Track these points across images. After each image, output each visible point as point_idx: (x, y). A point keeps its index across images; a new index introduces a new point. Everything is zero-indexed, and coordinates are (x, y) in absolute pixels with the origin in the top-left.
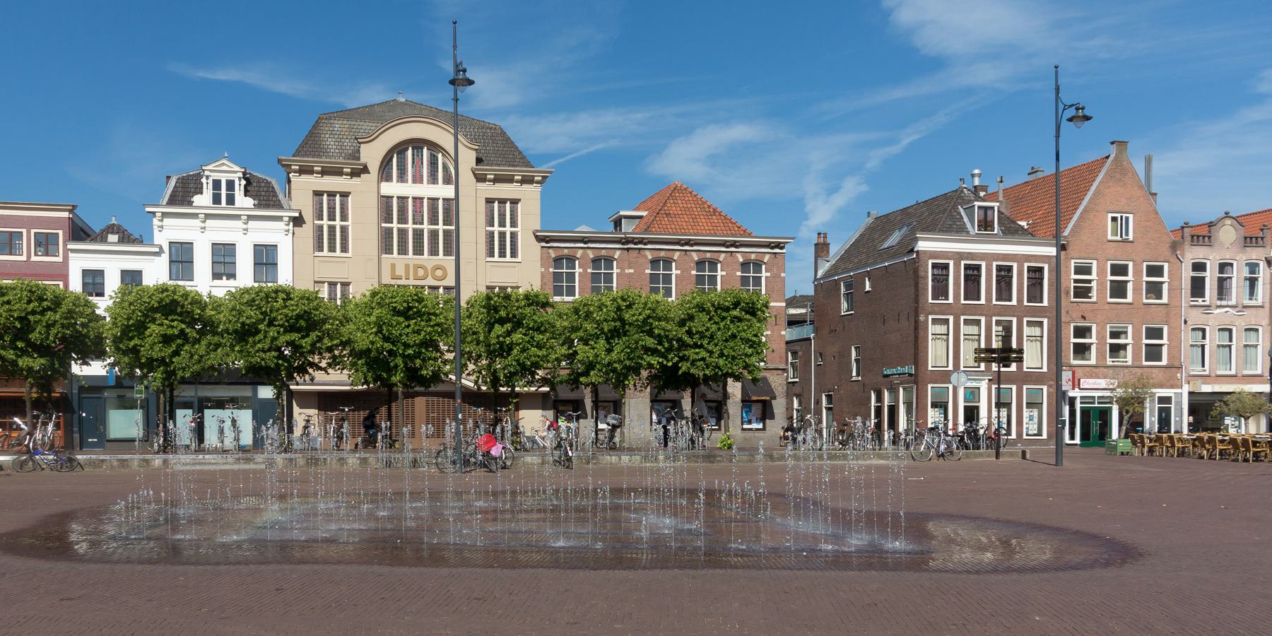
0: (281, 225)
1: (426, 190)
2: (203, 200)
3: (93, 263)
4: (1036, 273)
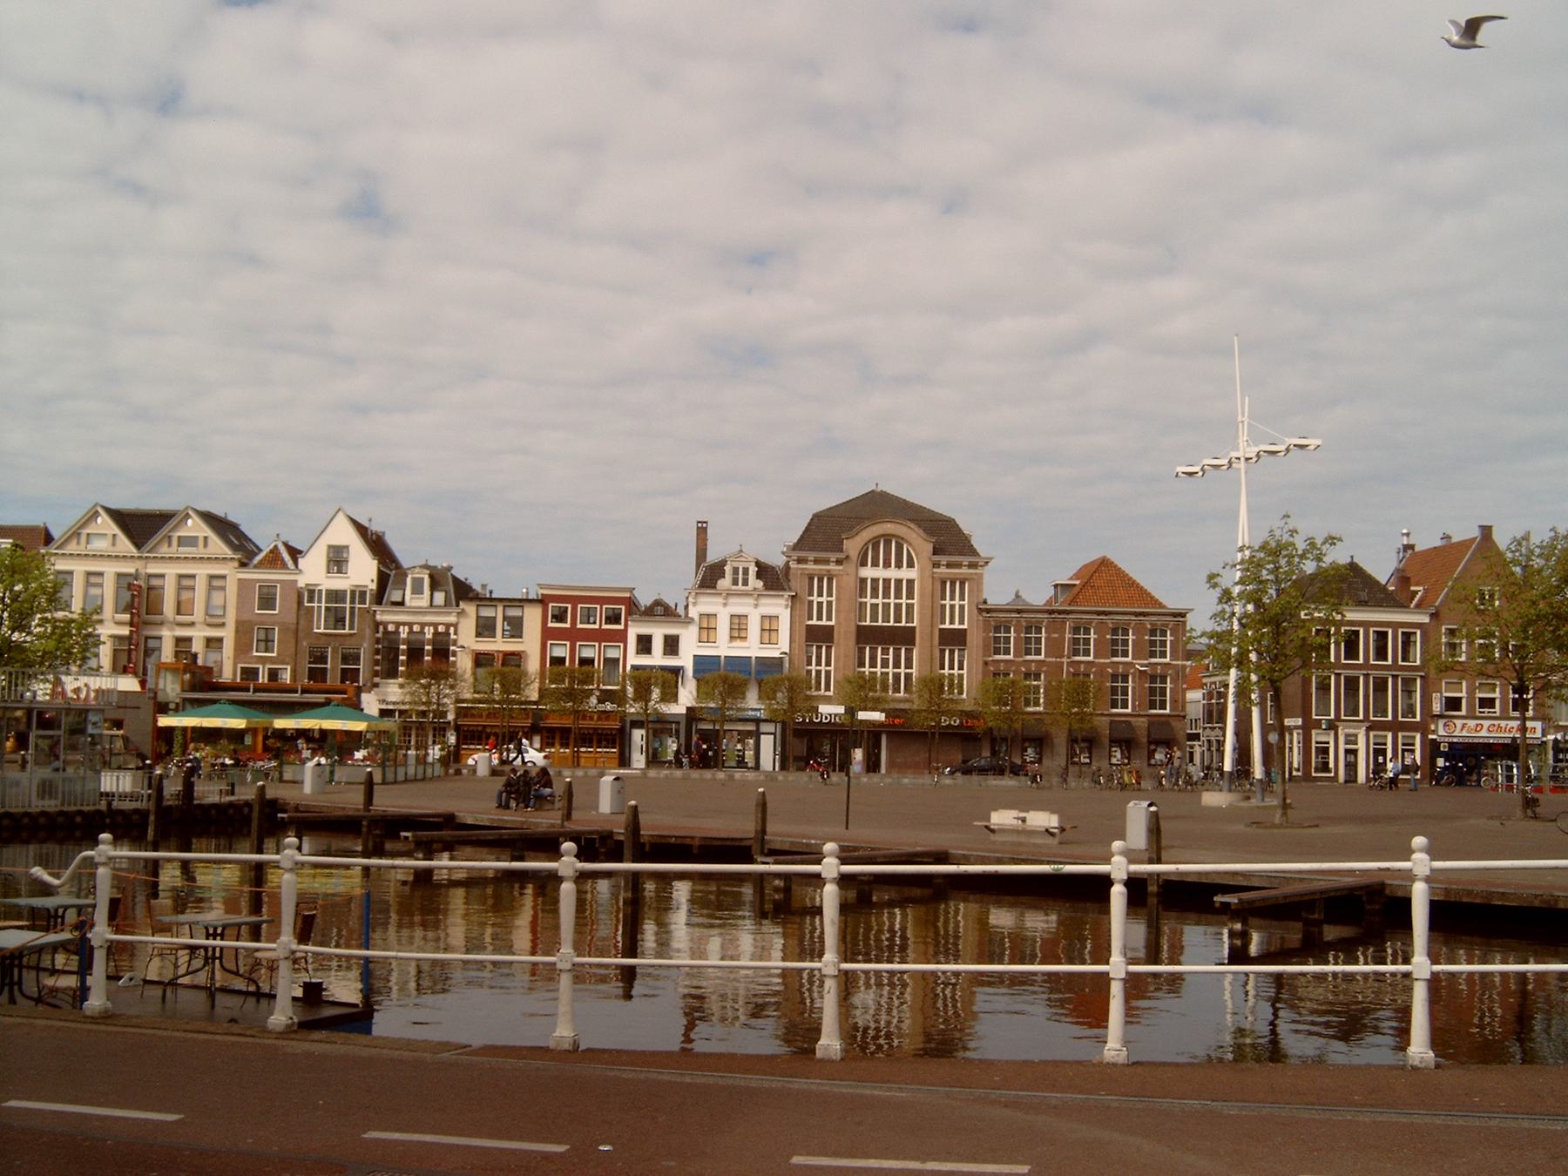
0: (782, 602)
1: (893, 573)
2: (725, 583)
3: (645, 631)
4: (1407, 637)
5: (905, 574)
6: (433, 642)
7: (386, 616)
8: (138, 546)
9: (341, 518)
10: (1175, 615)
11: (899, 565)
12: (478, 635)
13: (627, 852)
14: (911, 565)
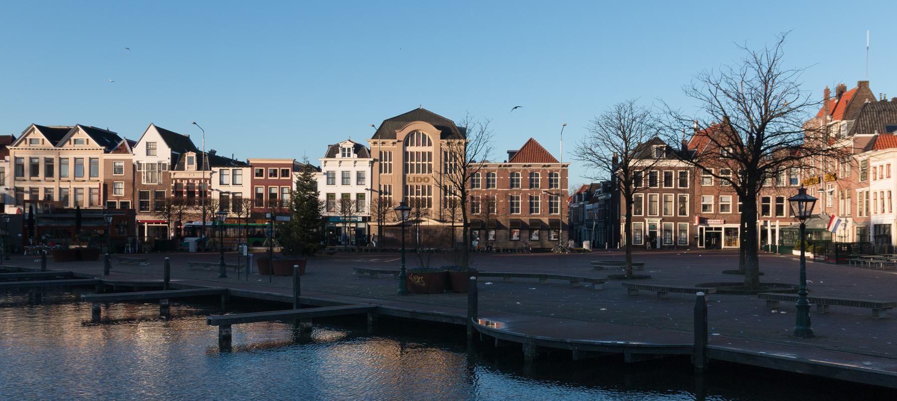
4: (683, 175)
5: (426, 149)
6: (187, 188)
7: (179, 175)
8: (55, 144)
9: (152, 128)
10: (564, 166)
11: (424, 145)
12: (140, 192)
13: (295, 307)
14: (430, 144)
